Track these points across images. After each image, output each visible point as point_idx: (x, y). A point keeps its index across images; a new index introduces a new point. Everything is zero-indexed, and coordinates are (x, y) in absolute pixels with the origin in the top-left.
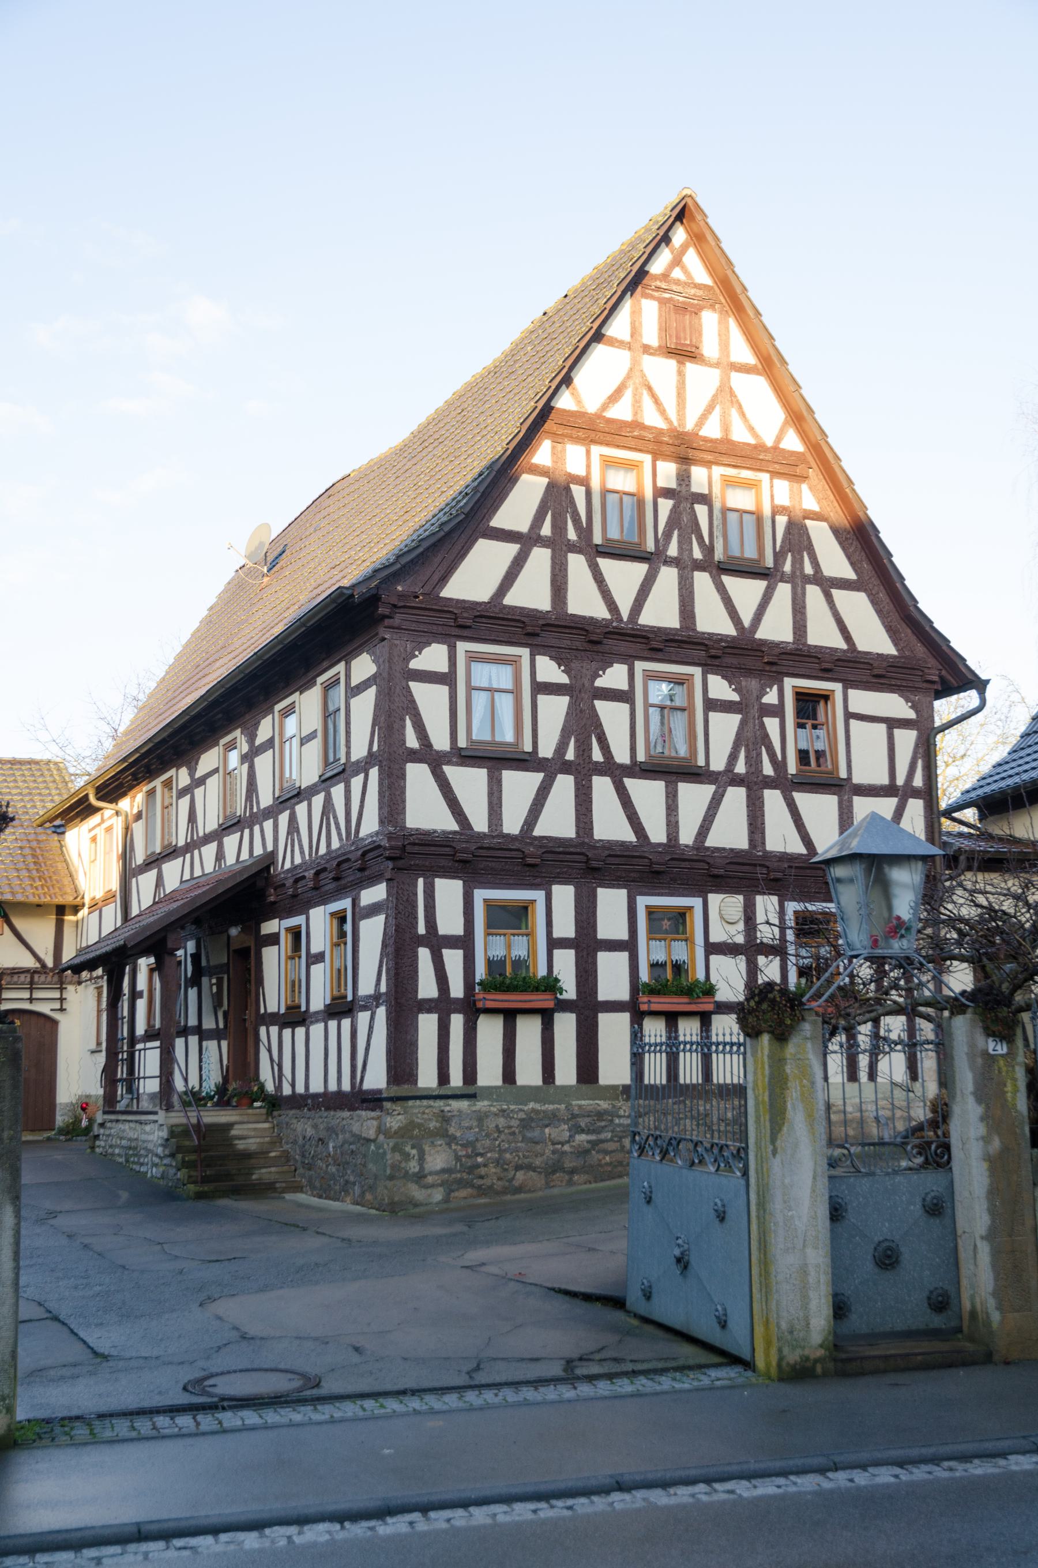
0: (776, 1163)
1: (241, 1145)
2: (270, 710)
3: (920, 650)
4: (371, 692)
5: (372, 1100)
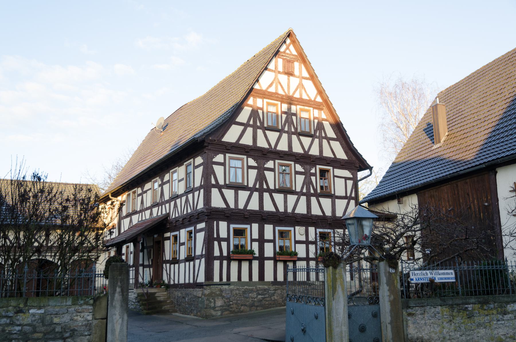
0: (334, 302)
1: (159, 299)
2: (169, 172)
3: (354, 158)
4: (201, 168)
5: (200, 286)
